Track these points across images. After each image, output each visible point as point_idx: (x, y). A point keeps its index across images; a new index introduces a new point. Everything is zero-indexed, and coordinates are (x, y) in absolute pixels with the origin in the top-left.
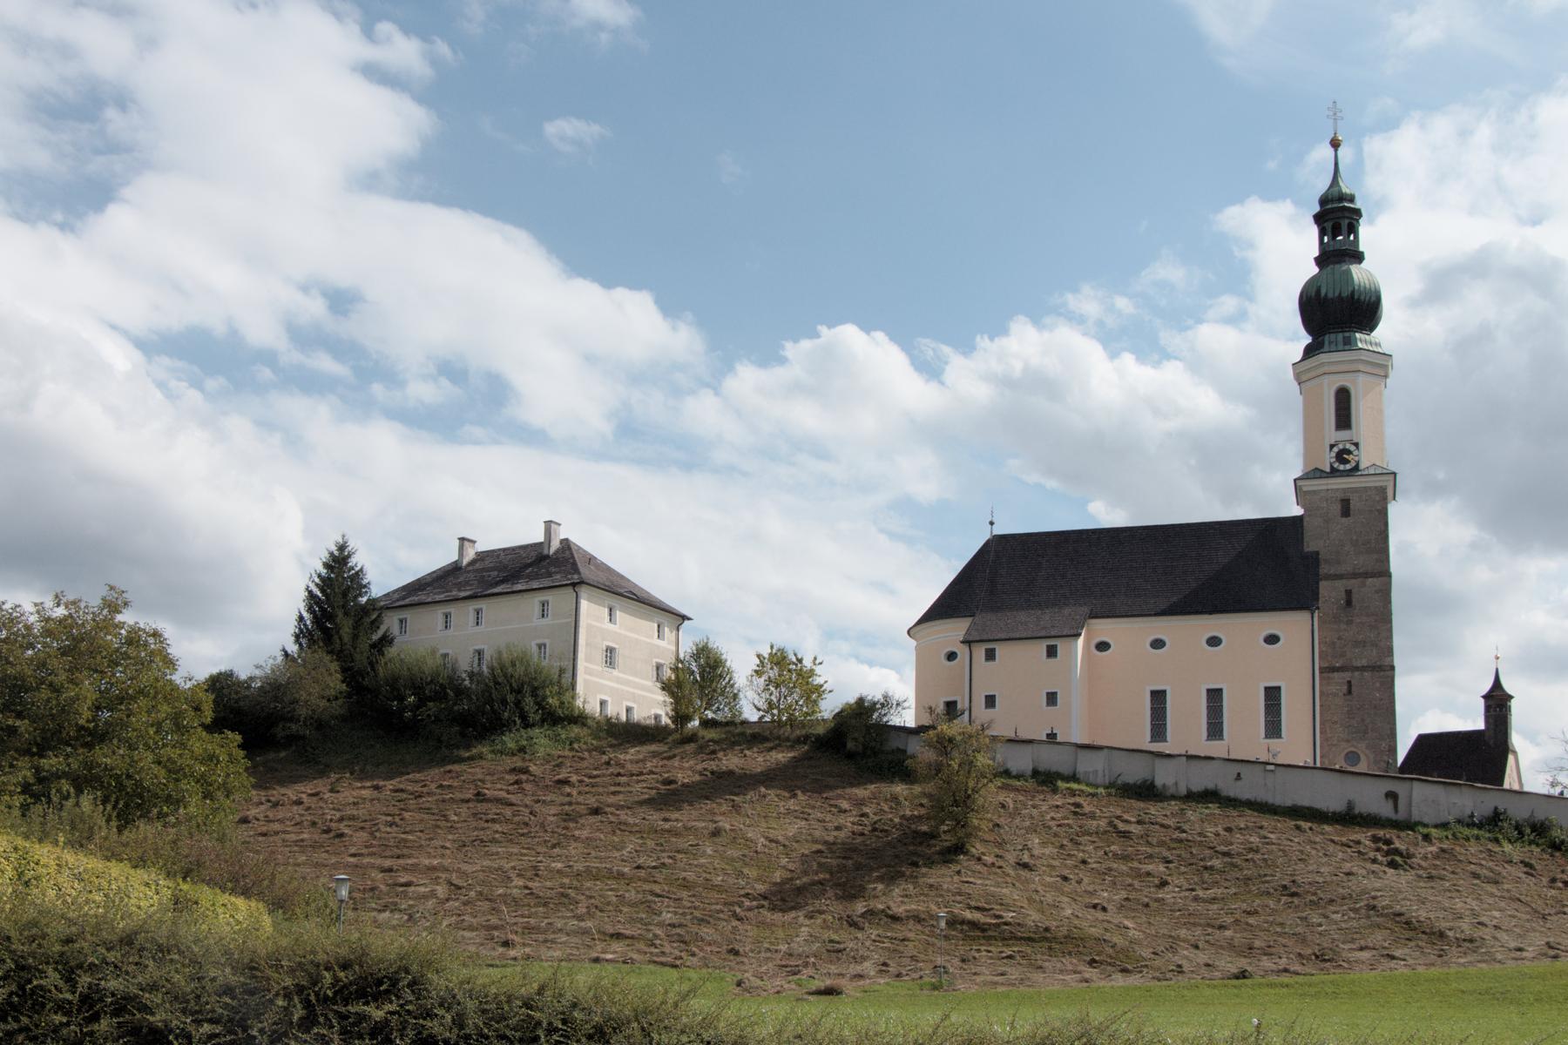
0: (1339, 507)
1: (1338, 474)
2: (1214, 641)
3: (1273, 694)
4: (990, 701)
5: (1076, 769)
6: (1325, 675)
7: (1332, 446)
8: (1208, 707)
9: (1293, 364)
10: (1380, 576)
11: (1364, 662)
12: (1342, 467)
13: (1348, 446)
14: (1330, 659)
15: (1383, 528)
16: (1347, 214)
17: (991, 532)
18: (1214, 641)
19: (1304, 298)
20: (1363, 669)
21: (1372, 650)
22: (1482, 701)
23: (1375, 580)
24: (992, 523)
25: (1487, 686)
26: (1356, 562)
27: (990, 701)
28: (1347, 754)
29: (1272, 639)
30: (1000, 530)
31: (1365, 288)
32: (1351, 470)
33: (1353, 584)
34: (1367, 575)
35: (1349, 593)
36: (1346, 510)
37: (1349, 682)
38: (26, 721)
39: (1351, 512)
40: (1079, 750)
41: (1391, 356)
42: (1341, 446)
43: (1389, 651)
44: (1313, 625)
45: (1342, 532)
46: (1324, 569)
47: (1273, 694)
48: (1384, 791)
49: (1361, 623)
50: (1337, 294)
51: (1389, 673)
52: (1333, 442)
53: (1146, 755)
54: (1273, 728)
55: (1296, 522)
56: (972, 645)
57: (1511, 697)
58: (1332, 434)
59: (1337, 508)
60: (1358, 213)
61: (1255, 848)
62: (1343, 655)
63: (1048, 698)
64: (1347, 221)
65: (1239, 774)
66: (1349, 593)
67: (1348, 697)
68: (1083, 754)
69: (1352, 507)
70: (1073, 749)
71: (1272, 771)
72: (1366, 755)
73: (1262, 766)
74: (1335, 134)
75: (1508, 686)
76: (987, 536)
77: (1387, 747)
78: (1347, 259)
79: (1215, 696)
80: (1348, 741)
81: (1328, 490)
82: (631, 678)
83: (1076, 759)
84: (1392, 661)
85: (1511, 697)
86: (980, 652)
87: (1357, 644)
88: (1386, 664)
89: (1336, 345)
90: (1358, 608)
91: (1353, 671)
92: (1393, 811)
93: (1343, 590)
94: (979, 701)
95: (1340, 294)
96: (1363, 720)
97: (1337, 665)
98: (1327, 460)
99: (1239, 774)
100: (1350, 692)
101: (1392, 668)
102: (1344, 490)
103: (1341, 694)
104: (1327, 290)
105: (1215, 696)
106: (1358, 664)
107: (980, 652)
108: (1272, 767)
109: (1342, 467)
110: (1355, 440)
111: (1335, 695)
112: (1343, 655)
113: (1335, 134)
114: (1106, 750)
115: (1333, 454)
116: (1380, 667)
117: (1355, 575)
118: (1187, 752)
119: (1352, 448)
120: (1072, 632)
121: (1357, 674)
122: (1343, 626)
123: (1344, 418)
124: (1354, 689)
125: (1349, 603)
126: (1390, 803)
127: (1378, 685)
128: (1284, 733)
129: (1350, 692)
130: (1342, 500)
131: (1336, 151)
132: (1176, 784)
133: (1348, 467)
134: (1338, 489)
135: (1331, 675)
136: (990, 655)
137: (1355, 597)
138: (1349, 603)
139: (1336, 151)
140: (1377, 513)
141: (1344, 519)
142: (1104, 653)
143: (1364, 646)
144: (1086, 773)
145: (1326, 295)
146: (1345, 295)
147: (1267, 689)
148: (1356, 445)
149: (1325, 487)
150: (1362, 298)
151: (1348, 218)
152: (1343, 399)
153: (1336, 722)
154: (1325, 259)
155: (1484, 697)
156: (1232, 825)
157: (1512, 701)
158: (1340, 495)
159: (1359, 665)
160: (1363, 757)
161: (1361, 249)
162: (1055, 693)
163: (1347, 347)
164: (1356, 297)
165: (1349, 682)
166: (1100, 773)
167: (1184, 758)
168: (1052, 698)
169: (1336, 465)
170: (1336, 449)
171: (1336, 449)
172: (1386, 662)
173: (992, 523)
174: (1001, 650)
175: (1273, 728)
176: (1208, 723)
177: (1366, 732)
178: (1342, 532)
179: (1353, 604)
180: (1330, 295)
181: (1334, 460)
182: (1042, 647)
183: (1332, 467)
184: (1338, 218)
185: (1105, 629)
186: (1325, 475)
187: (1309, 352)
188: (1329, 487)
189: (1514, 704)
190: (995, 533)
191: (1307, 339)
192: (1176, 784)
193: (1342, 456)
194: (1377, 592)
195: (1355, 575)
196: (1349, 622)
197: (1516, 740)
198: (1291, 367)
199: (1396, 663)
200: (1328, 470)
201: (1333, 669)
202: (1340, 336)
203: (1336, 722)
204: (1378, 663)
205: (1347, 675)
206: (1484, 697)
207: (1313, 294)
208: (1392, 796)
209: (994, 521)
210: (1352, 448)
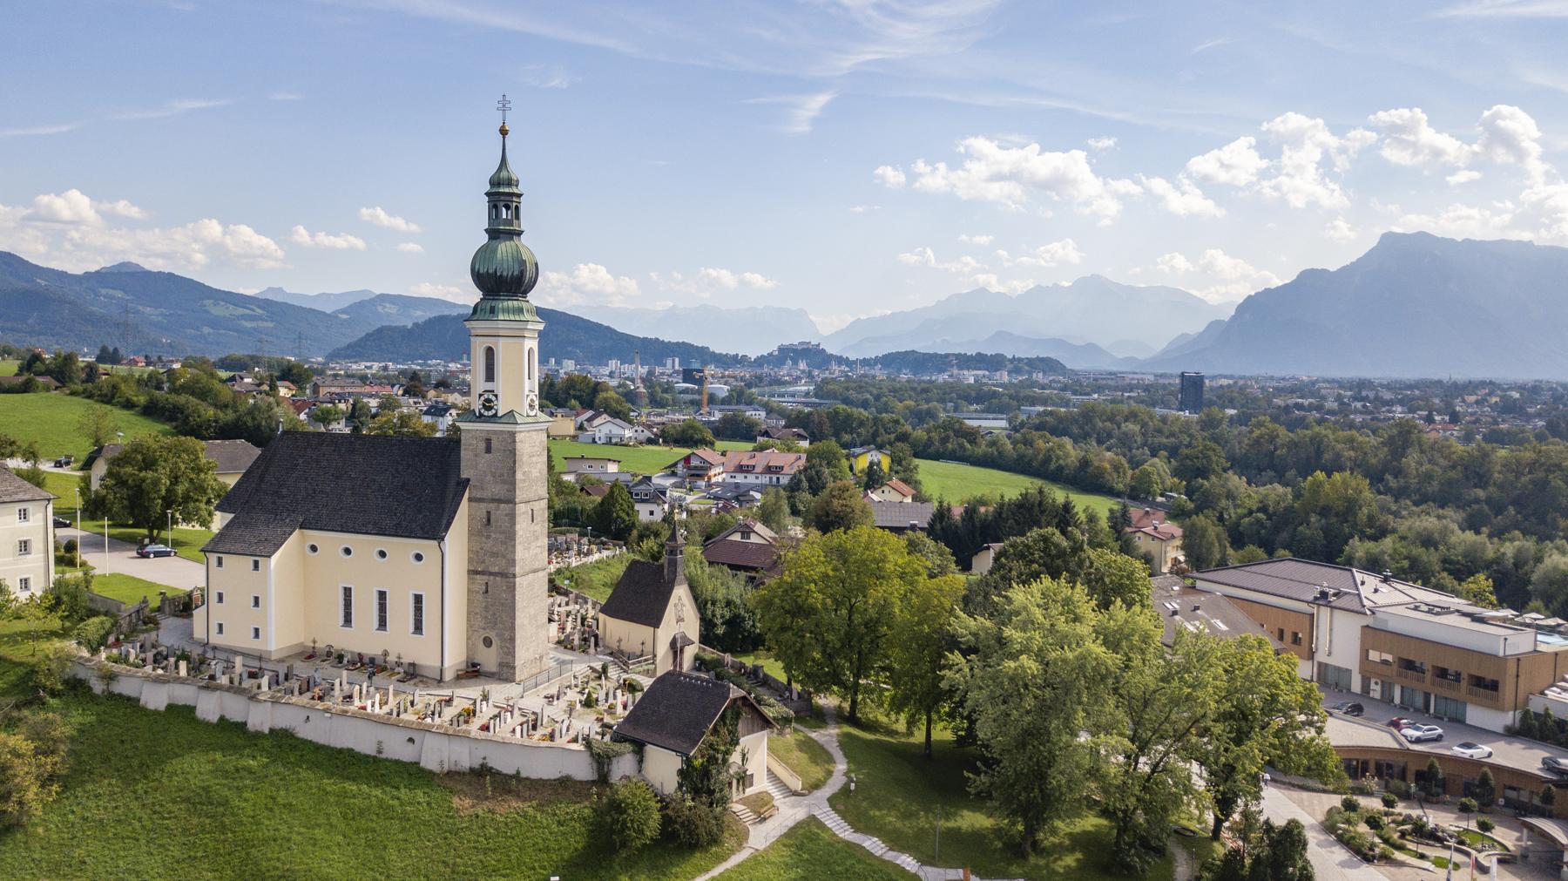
2: (220, 598)
3: (418, 599)
7: (480, 395)
11: (496, 569)
13: (491, 397)
16: (502, 198)
31: (501, 276)
32: (492, 416)
33: (492, 506)
34: (500, 501)
35: (489, 513)
36: (488, 442)
38: (1325, 542)
42: (486, 396)
47: (418, 599)
59: (482, 445)
66: (489, 513)
80: (484, 629)
82: (887, 739)
96: (494, 614)
100: (487, 592)
109: (486, 413)
111: (478, 592)
112: (483, 562)
115: (481, 402)
117: (493, 500)
119: (494, 399)
121: (492, 578)
129: (487, 592)
131: (504, 138)
137: (492, 517)
139: (504, 138)
142: (1052, 355)
148: (496, 396)
150: (505, 274)
153: (477, 614)
154: (494, 234)
156: (484, 721)
158: (484, 435)
171: (482, 398)
185: (315, 536)
195: (493, 500)
196: (488, 537)
201: (476, 572)
203: (477, 614)
210: (494, 399)
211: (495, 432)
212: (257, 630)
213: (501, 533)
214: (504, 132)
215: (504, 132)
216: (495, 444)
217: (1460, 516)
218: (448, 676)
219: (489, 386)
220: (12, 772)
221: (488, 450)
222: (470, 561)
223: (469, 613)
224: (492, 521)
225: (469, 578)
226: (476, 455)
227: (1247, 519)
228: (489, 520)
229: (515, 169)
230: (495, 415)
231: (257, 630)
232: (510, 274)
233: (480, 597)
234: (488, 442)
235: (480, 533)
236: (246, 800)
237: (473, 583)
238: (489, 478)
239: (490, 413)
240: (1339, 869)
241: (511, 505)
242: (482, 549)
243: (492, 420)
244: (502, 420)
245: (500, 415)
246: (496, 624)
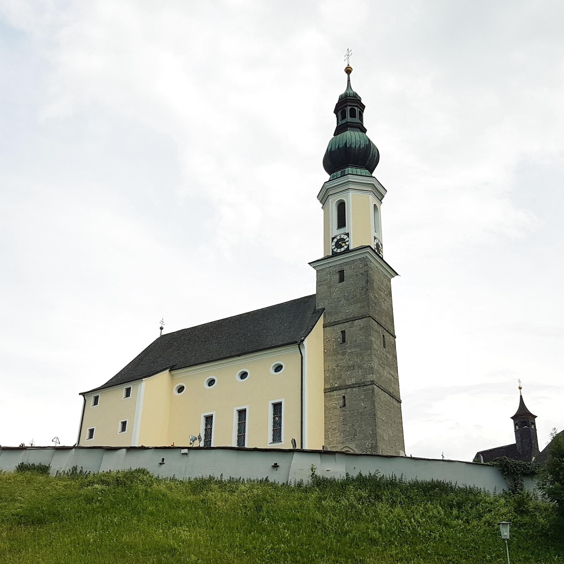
3: (277, 407)
6: (328, 394)
7: (333, 239)
9: (322, 208)
11: (353, 381)
14: (331, 381)
17: (161, 334)
25: (514, 409)
30: (164, 332)
31: (350, 147)
35: (343, 332)
37: (344, 397)
41: (387, 191)
42: (338, 238)
47: (277, 407)
49: (350, 352)
52: (333, 236)
58: (335, 232)
59: (337, 277)
61: (484, 531)
64: (349, 108)
66: (343, 332)
69: (345, 275)
71: (186, 454)
75: (532, 408)
79: (242, 413)
80: (343, 443)
83: (52, 460)
91: (346, 389)
108: (186, 451)
109: (339, 251)
111: (335, 408)
115: (334, 243)
117: (347, 321)
118: (32, 445)
119: (345, 237)
121: (349, 390)
123: (342, 223)
127: (363, 397)
128: (283, 439)
133: (343, 249)
135: (332, 393)
143: (354, 369)
151: (350, 106)
155: (512, 418)
157: (536, 419)
158: (339, 269)
165: (344, 397)
170: (335, 240)
171: (335, 240)
173: (161, 328)
176: (238, 436)
181: (334, 247)
183: (333, 251)
188: (330, 265)
190: (163, 334)
191: (327, 177)
195: (347, 321)
196: (344, 354)
198: (322, 209)
201: (333, 389)
206: (512, 418)
209: (163, 326)
211: (347, 263)
212: (124, 424)
213: (355, 347)
214: (348, 71)
215: (348, 71)
218: (509, 524)
220: (411, 481)
221: (342, 279)
222: (326, 380)
223: (326, 431)
225: (326, 397)
228: (344, 340)
231: (124, 424)
232: (358, 146)
233: (338, 412)
235: (336, 353)
237: (330, 400)
240: (267, 476)
242: (337, 366)
246: (355, 435)
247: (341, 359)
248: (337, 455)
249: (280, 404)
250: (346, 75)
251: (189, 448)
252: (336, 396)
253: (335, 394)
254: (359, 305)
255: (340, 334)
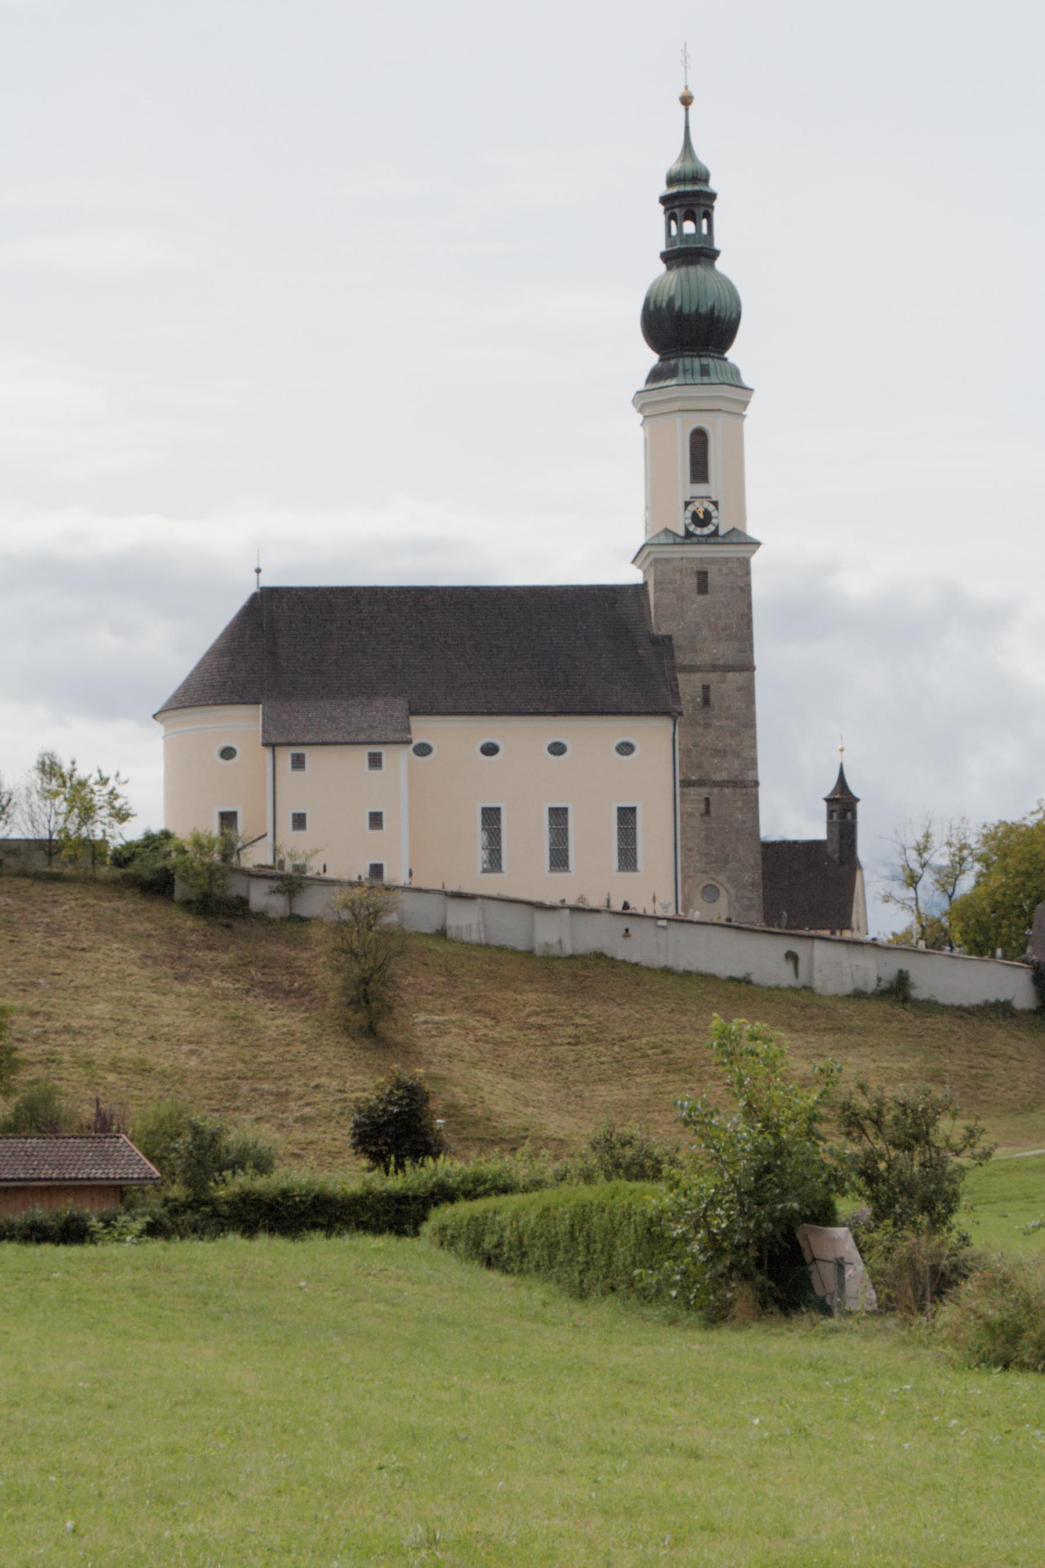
0: (695, 581)
1: (694, 540)
3: (627, 816)
4: (299, 821)
5: (445, 919)
8: (550, 829)
10: (743, 671)
11: (724, 776)
12: (698, 531)
15: (746, 610)
18: (557, 749)
19: (652, 308)
20: (722, 784)
21: (733, 762)
22: (825, 804)
23: (737, 674)
24: (258, 571)
25: (829, 786)
26: (715, 651)
27: (299, 821)
28: (705, 887)
29: (626, 748)
30: (270, 580)
33: (712, 678)
34: (727, 668)
35: (706, 688)
36: (702, 577)
39: (709, 589)
40: (448, 900)
43: (753, 763)
44: (674, 734)
45: (698, 612)
46: (681, 658)
47: (627, 816)
48: (785, 951)
50: (694, 308)
51: (753, 790)
52: (688, 499)
53: (525, 907)
54: (627, 859)
55: (638, 591)
56: (277, 749)
57: (858, 800)
59: (692, 582)
60: (713, 196)
62: (700, 766)
63: (371, 820)
65: (627, 930)
66: (706, 688)
67: (707, 818)
68: (453, 906)
70: (441, 897)
71: (663, 927)
72: (727, 891)
73: (651, 922)
74: (686, 87)
76: (253, 589)
77: (750, 880)
78: (702, 259)
79: (558, 816)
80: (705, 872)
81: (682, 558)
83: (446, 911)
84: (756, 775)
85: (858, 800)
86: (285, 757)
87: (717, 752)
88: (750, 779)
89: (692, 374)
90: (717, 708)
92: (793, 975)
93: (699, 685)
94: (286, 821)
95: (698, 308)
97: (693, 778)
98: (679, 523)
99: (627, 930)
100: (707, 812)
101: (756, 784)
102: (701, 560)
103: (697, 814)
104: (682, 303)
105: (558, 816)
106: (717, 777)
107: (285, 757)
108: (663, 923)
109: (698, 531)
110: (714, 499)
112: (700, 766)
113: (686, 87)
114: (479, 901)
116: (742, 782)
117: (714, 668)
120: (397, 737)
121: (716, 790)
122: (700, 730)
123: (699, 471)
124: (712, 809)
125: (706, 701)
126: (790, 967)
127: (740, 804)
128: (640, 865)
129: (707, 812)
130: (699, 573)
131: (687, 110)
132: (560, 942)
134: (693, 559)
136: (298, 762)
138: (706, 701)
139: (687, 110)
140: (739, 591)
141: (700, 598)
144: (458, 927)
145: (681, 308)
146: (703, 310)
147: (621, 810)
149: (680, 555)
150: (723, 314)
152: (699, 440)
158: (696, 567)
159: (719, 779)
160: (723, 893)
161: (717, 245)
162: (380, 814)
163: (706, 380)
164: (716, 313)
165: (707, 800)
166: (475, 928)
167: (567, 911)
168: (376, 820)
169: (692, 528)
172: (750, 776)
173: (258, 571)
174: (312, 756)
175: (627, 859)
177: (726, 862)
178: (698, 612)
179: (711, 703)
180: (686, 310)
181: (690, 521)
182: (362, 754)
183: (687, 530)
184: (692, 205)
186: (679, 540)
187: (655, 376)
188: (685, 555)
189: (860, 807)
191: (652, 358)
192: (560, 942)
193: (702, 520)
194: (739, 689)
195: (714, 668)
197: (863, 853)
199: (761, 779)
200: (682, 532)
202: (697, 363)
204: (740, 778)
205: (705, 791)
206: (826, 800)
207: (664, 304)
208: (792, 957)
211: (714, 561)
214: (686, 101)
215: (686, 101)
216: (713, 579)
217: (489, 1235)
219: (700, 489)
221: (703, 587)
224: (713, 700)
226: (682, 598)
227: (321, 1221)
229: (705, 156)
230: (715, 533)
234: (702, 577)
236: (589, 1058)
238: (705, 632)
239: (706, 531)
241: (746, 673)
242: (696, 745)
243: (712, 540)
244: (728, 540)
245: (722, 532)
247: (702, 735)
248: (866, 947)
249: (633, 810)
250: (683, 107)
251: (668, 919)
252: (694, 795)
253: (692, 793)
254: (736, 644)
255: (701, 689)
